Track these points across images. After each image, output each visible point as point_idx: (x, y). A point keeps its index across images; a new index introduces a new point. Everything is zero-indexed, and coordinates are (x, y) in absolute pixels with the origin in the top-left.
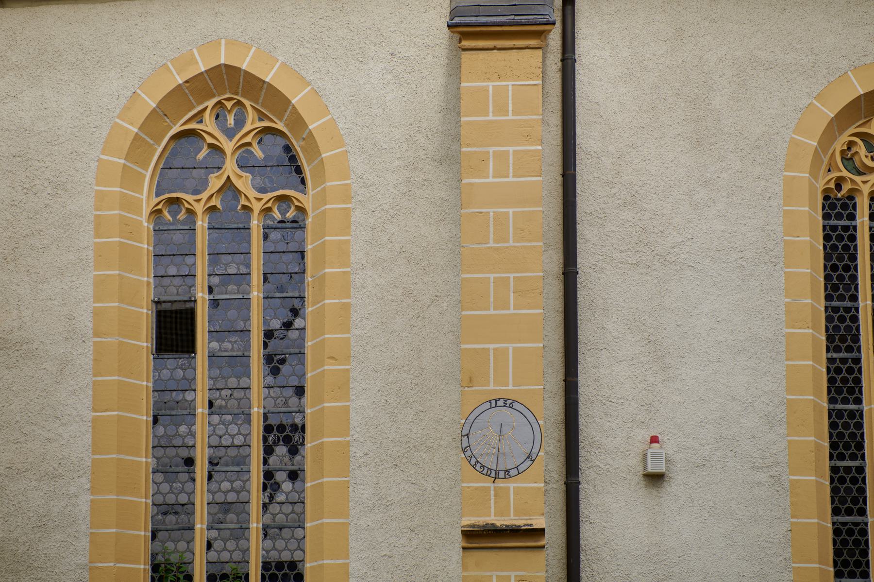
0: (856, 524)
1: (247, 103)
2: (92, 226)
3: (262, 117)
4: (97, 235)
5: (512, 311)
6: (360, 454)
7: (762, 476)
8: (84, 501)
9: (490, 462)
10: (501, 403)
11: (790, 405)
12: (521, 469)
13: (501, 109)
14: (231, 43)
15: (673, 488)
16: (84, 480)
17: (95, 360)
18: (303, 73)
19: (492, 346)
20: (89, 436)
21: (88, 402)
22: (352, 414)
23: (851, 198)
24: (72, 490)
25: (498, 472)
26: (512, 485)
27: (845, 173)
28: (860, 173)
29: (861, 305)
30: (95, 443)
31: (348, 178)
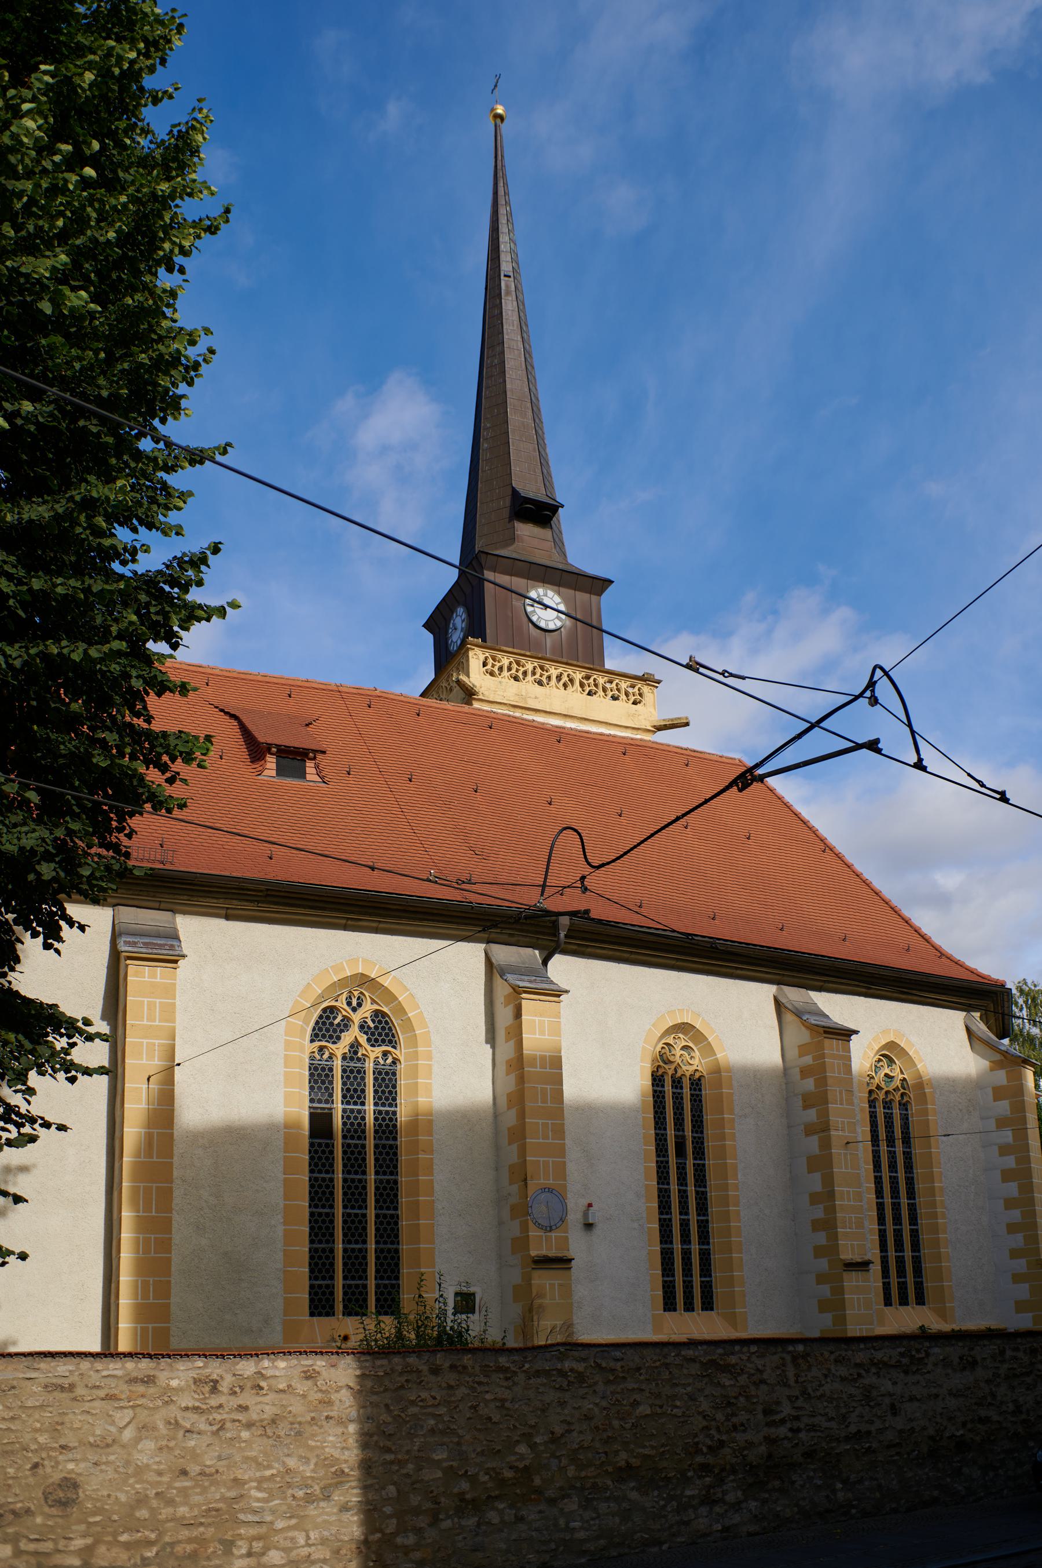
0: (669, 1249)
1: (367, 994)
2: (282, 1061)
3: (373, 1002)
4: (286, 1067)
5: (550, 1141)
6: (440, 1207)
7: (636, 1225)
8: (280, 1229)
9: (545, 1223)
10: (547, 1190)
11: (647, 1186)
12: (558, 1225)
13: (542, 1033)
14: (365, 961)
15: (597, 1231)
16: (279, 1217)
17: (285, 1143)
18: (405, 983)
19: (542, 1159)
20: (282, 1189)
21: (281, 1169)
22: (435, 1184)
23: (662, 1076)
24: (273, 1222)
25: (551, 1227)
26: (553, 1234)
27: (661, 1064)
28: (666, 1063)
29: (668, 1132)
30: (285, 1194)
31: (430, 1047)
